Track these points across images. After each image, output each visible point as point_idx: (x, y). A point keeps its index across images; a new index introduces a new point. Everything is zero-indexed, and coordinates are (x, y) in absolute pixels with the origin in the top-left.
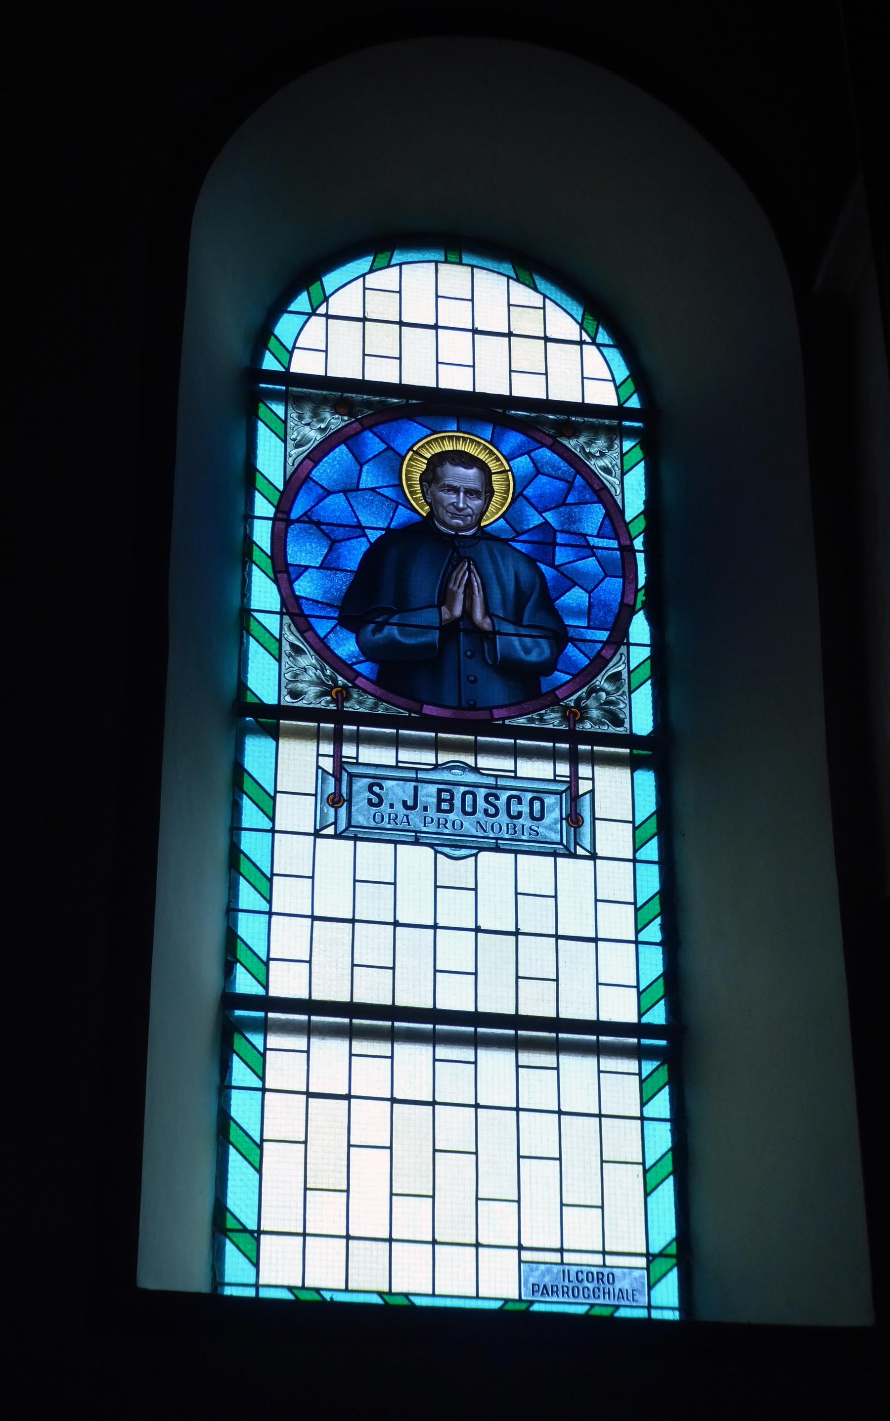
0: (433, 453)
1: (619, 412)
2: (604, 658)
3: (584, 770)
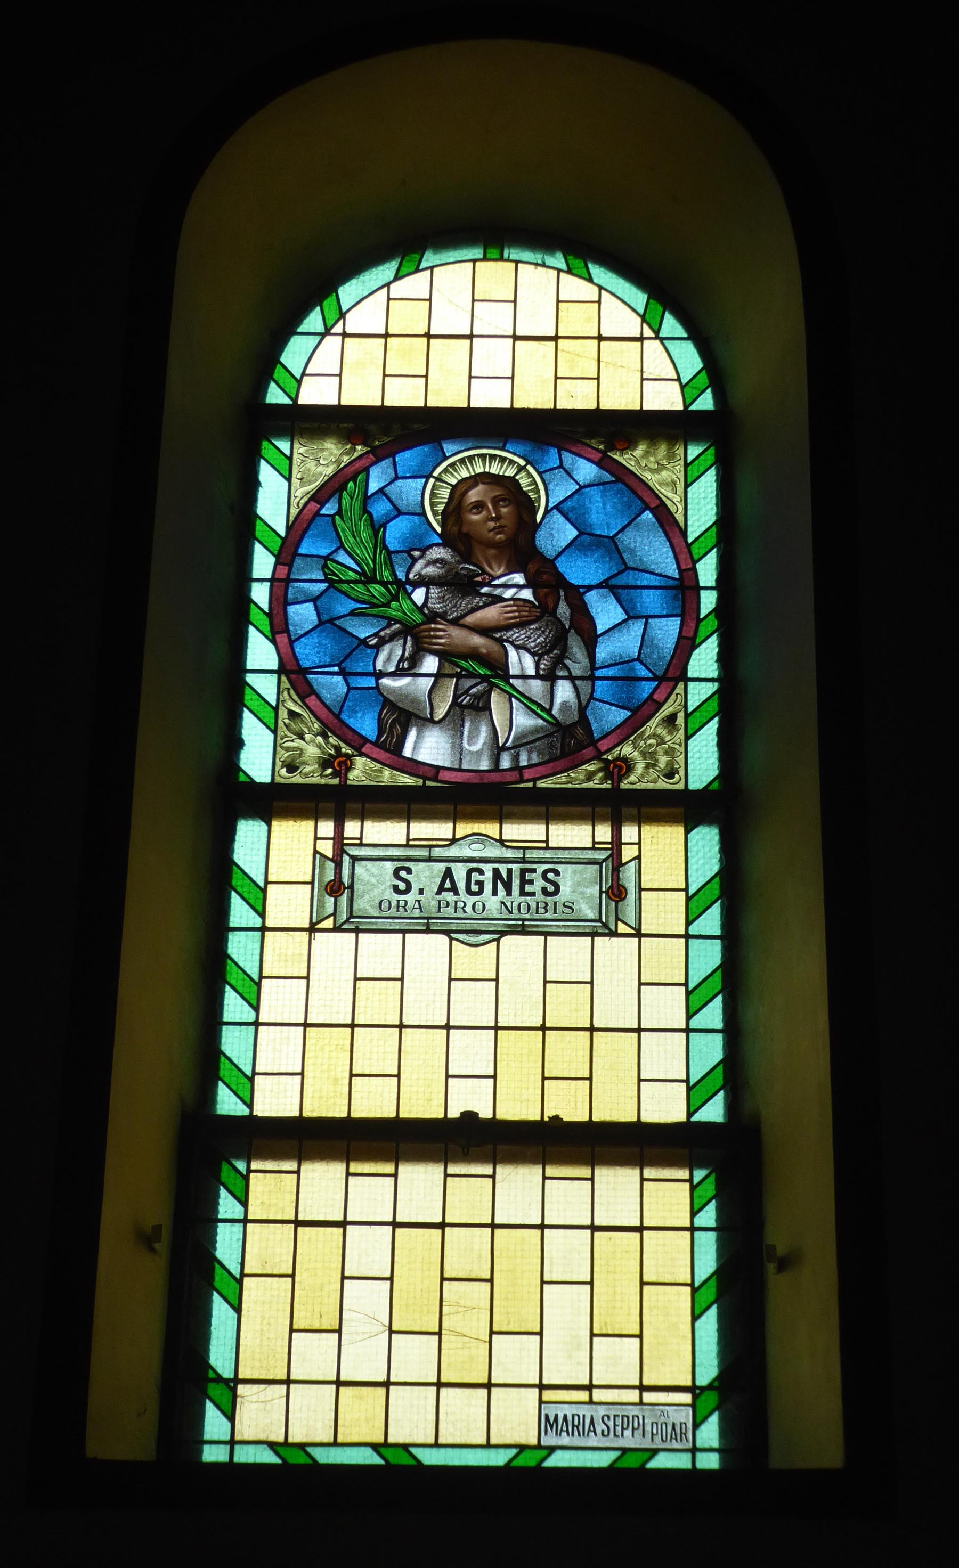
0: (460, 478)
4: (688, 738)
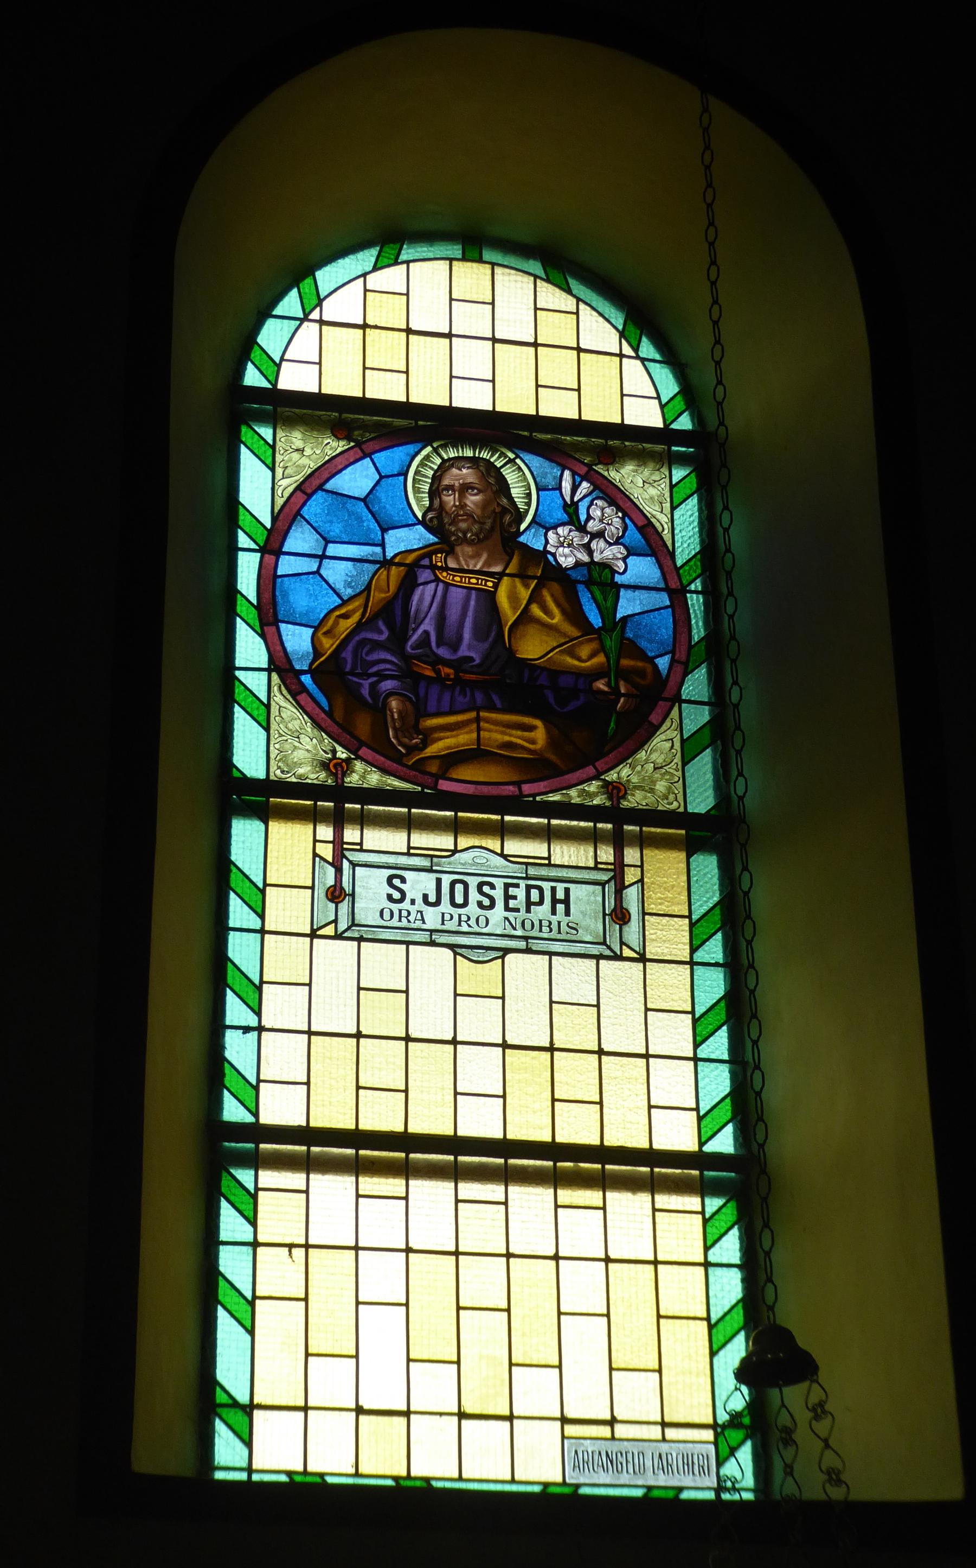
1: (665, 435)
3: (631, 855)
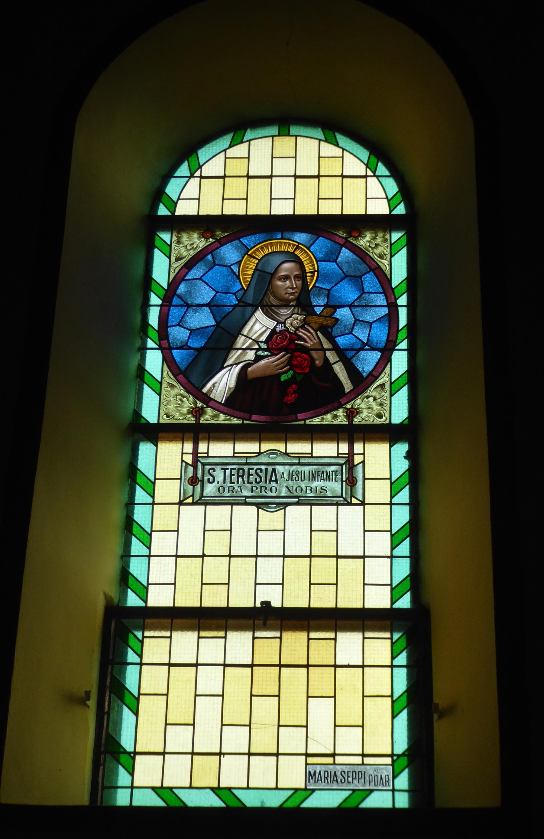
2: (374, 376)
4: (391, 396)
